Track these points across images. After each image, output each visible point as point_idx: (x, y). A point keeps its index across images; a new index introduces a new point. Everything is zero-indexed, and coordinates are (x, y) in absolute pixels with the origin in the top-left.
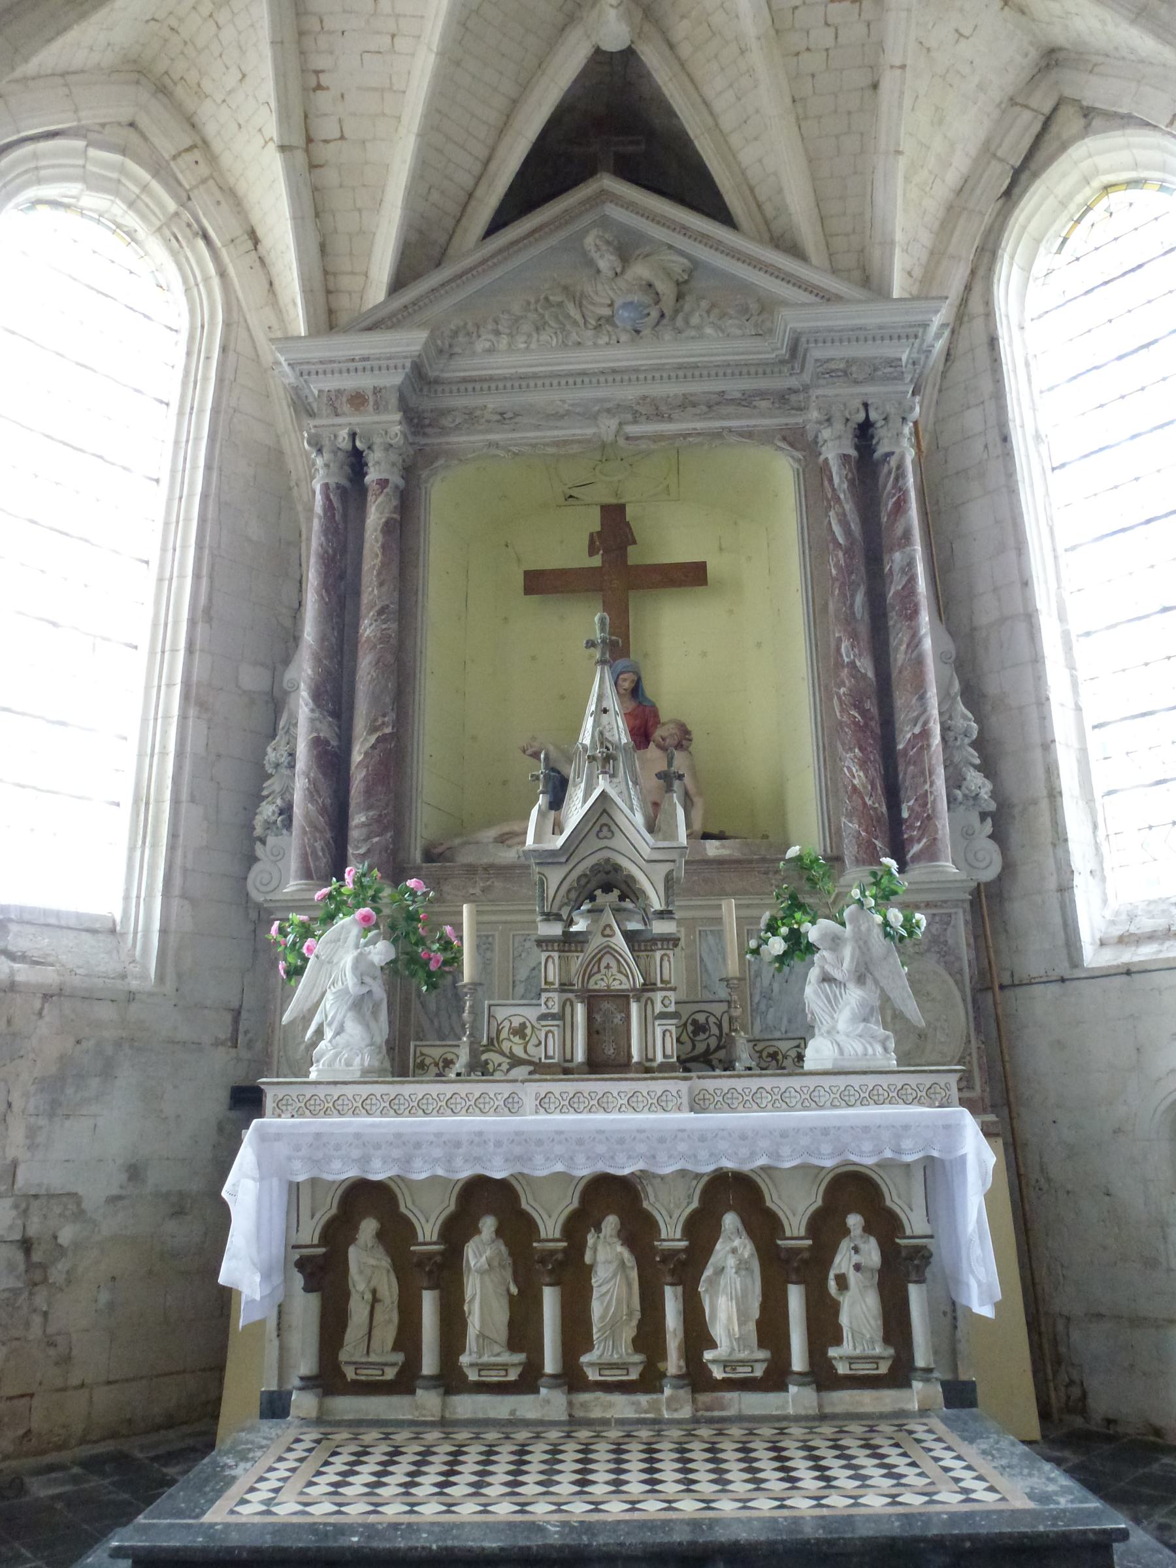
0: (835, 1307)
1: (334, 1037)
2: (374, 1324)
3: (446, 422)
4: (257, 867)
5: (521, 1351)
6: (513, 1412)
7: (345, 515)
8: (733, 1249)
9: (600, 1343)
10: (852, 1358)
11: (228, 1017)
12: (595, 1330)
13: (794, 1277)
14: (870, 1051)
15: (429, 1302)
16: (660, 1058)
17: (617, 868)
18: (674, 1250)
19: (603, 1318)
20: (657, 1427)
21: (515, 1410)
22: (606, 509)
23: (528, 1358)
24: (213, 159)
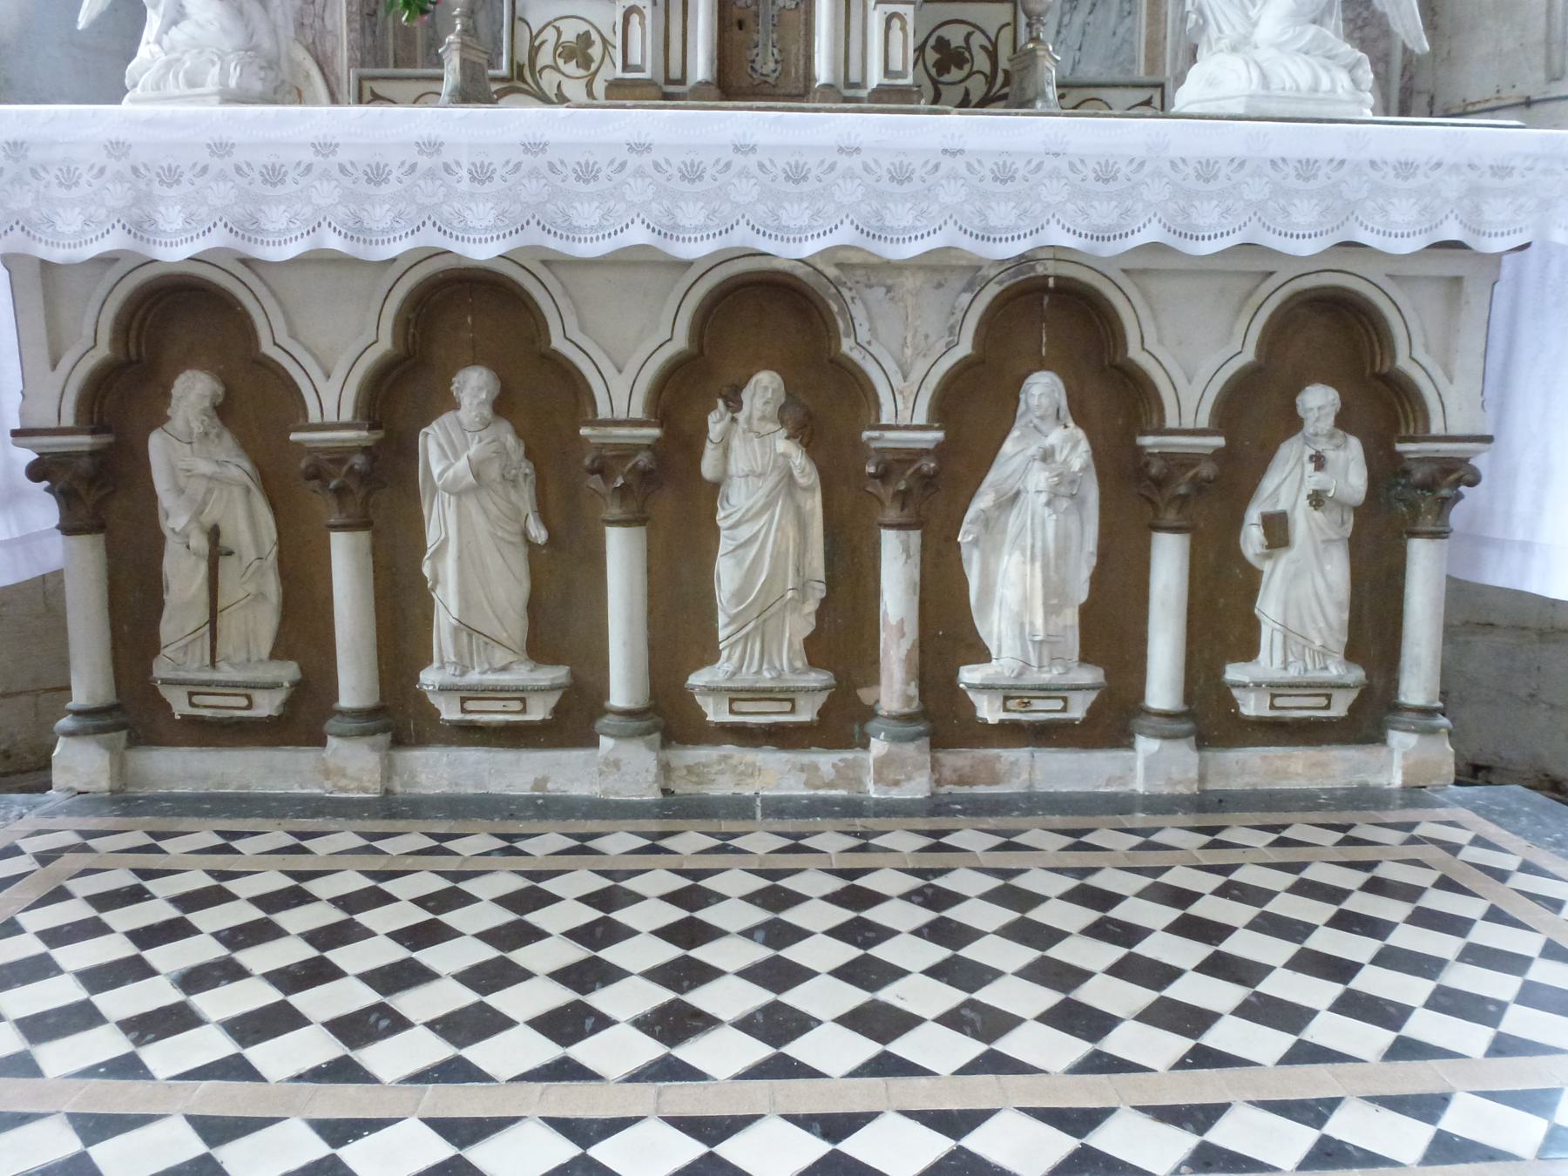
0: (1251, 582)
1: (165, 30)
2: (220, 605)
5: (555, 661)
6: (540, 783)
8: (1043, 457)
9: (732, 646)
10: (1279, 686)
12: (722, 619)
13: (1171, 516)
14: (1325, 83)
15: (346, 561)
16: (875, 78)
18: (909, 451)
19: (739, 595)
20: (859, 824)
21: (545, 780)
23: (572, 674)
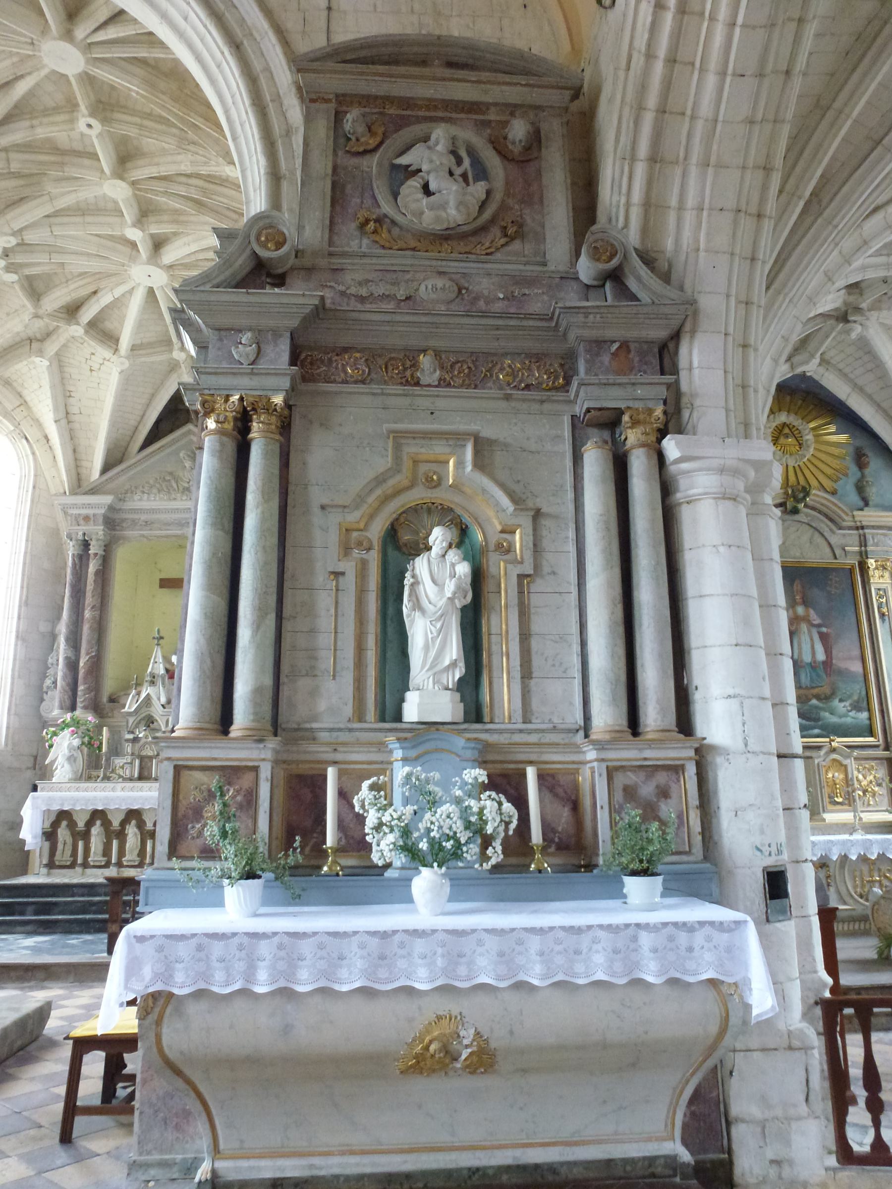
3: (124, 525)
4: (44, 703)
7: (81, 567)
11: (32, 759)
15: (81, 844)
17: (152, 717)
22: (161, 586)
24: (29, 408)
